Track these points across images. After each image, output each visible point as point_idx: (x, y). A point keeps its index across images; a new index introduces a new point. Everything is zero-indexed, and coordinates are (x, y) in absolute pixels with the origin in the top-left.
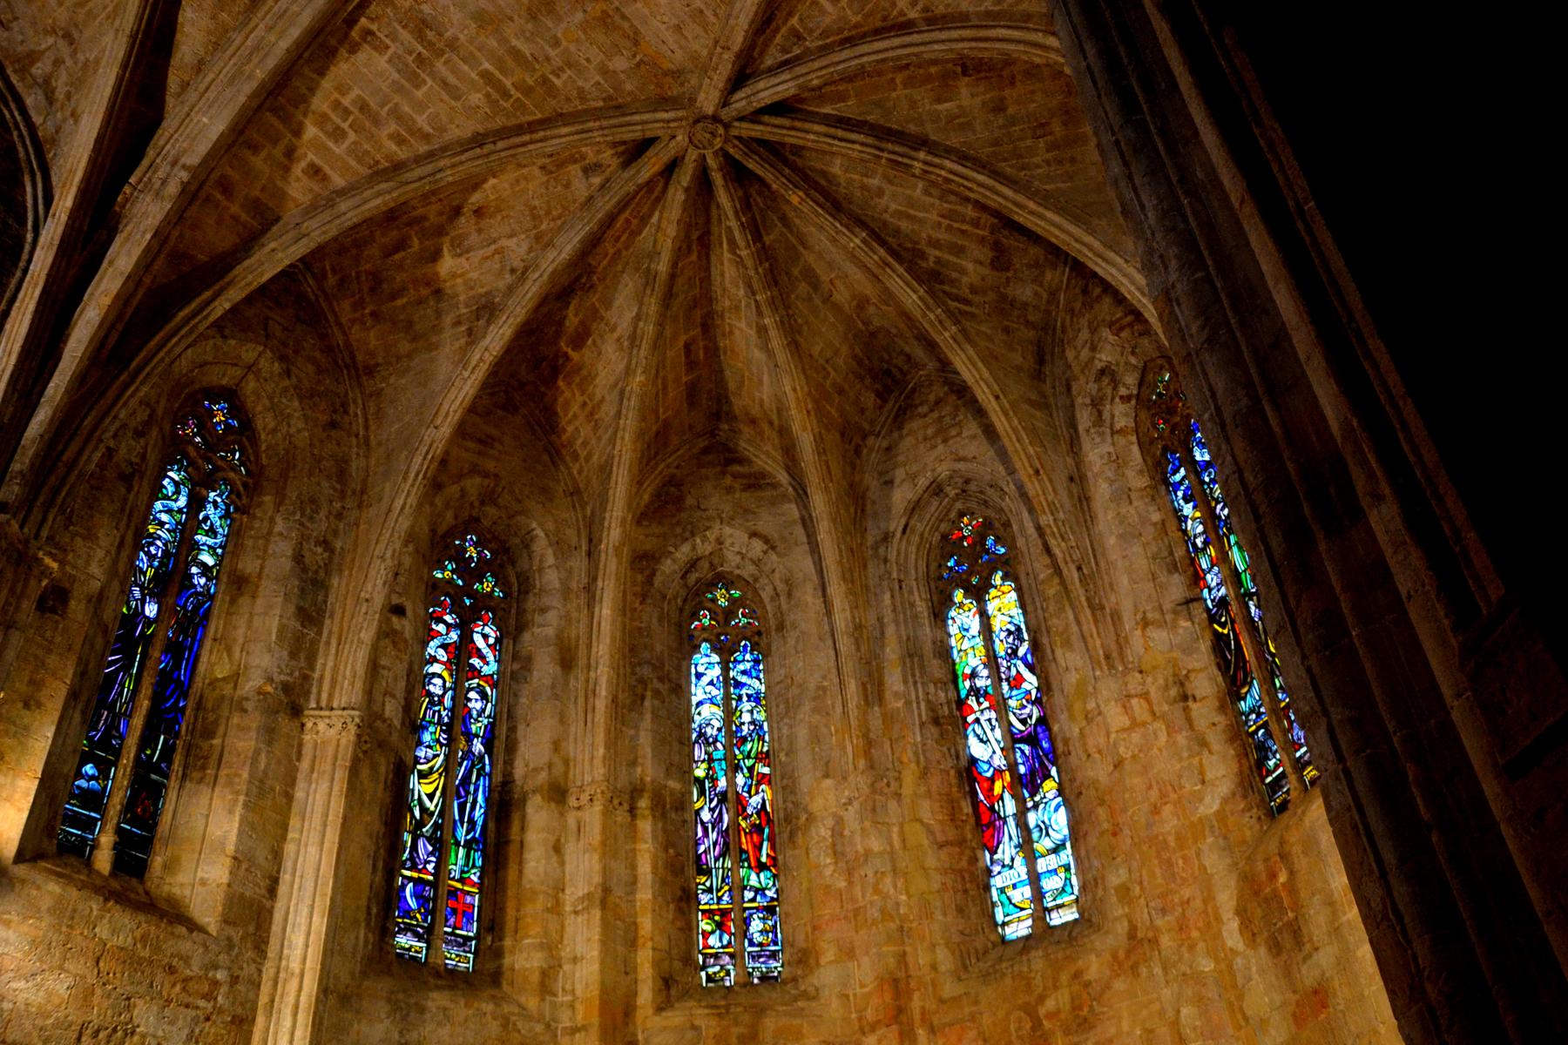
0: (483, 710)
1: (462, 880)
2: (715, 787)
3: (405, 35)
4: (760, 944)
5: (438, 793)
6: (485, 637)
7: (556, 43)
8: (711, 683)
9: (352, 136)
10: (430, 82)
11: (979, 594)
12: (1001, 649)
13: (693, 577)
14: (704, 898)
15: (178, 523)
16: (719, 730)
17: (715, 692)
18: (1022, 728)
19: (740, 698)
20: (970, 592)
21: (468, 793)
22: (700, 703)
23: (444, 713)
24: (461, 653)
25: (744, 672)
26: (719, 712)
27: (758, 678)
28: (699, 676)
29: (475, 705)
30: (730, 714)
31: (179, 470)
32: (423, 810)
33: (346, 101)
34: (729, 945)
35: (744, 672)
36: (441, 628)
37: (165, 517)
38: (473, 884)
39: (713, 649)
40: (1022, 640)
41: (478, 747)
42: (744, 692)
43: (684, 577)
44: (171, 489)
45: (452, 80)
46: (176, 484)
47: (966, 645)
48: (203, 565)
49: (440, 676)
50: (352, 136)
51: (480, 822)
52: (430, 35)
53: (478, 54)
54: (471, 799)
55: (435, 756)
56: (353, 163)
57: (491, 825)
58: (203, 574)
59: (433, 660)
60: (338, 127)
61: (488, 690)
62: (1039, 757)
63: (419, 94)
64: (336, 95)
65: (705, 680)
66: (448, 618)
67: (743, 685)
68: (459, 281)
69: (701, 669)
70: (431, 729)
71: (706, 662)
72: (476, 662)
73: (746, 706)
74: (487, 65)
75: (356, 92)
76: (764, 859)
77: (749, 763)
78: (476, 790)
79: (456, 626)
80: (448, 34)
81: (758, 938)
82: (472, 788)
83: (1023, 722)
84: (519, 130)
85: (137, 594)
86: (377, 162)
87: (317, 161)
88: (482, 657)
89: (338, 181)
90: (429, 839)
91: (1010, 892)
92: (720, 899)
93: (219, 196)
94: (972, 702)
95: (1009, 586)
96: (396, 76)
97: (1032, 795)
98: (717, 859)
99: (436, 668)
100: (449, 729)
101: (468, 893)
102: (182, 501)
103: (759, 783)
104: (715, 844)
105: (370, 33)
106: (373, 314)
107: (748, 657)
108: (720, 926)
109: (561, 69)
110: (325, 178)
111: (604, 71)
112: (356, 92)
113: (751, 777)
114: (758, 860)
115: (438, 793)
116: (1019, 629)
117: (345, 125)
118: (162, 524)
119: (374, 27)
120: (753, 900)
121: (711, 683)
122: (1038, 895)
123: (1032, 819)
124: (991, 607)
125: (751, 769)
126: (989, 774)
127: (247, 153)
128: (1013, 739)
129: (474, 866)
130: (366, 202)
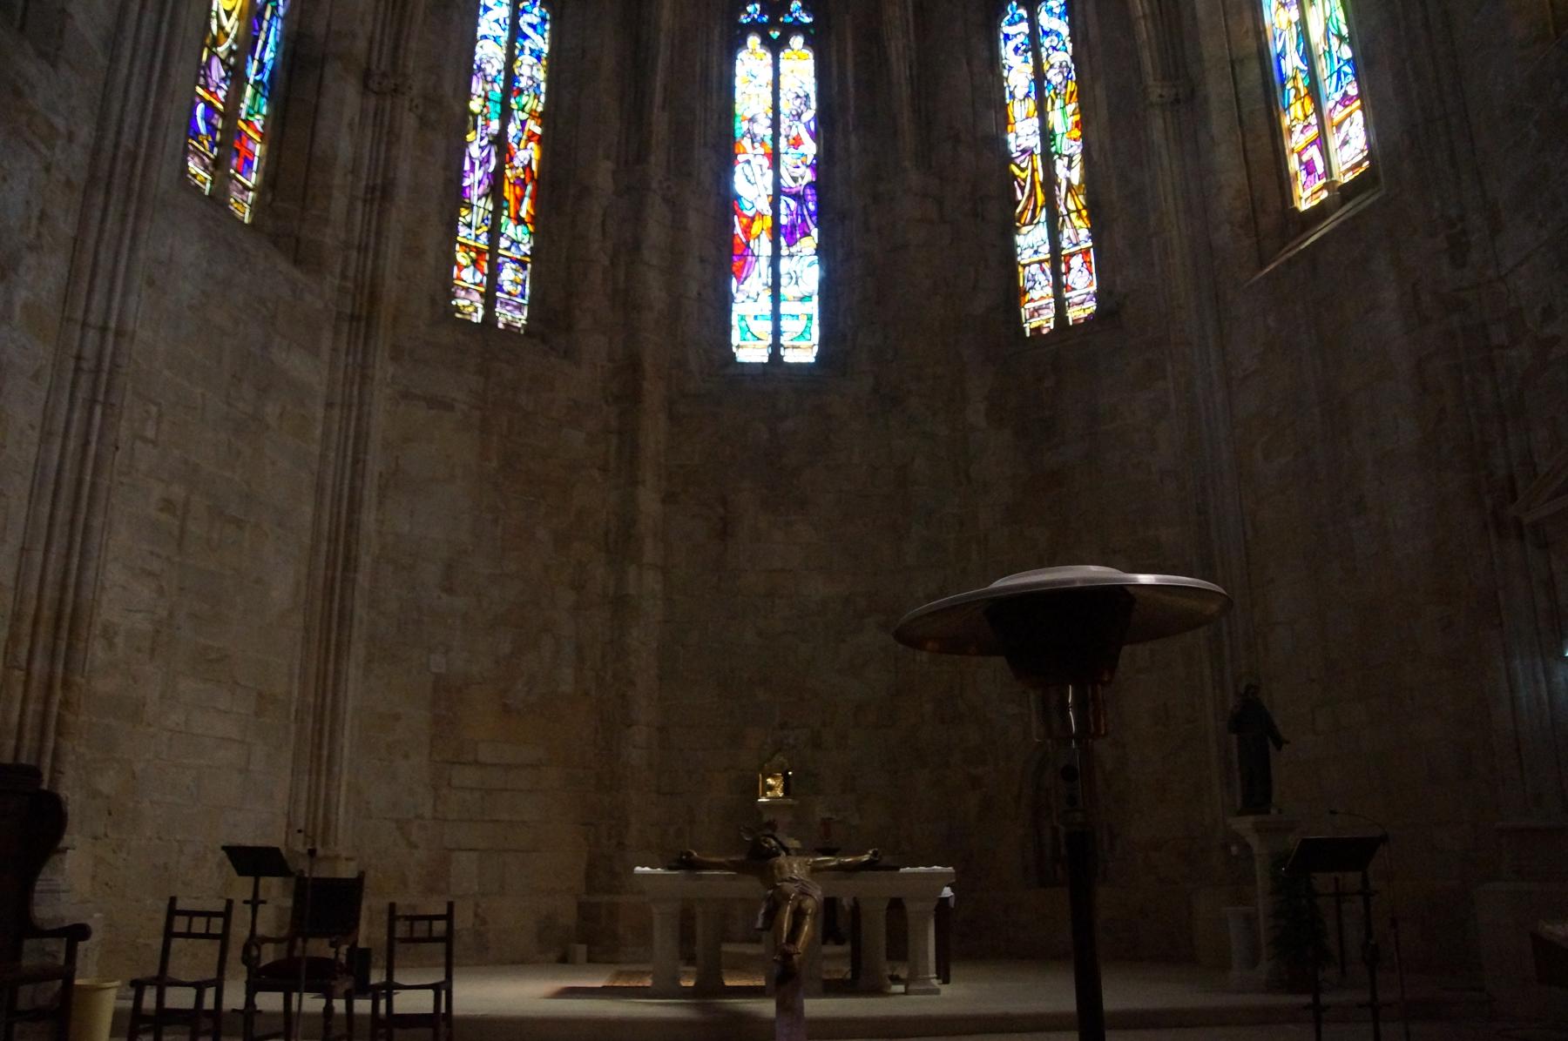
1: (246, 122)
2: (487, 126)
4: (509, 293)
5: (235, 15)
8: (497, 21)
11: (776, 48)
12: (786, 107)
14: (463, 231)
17: (499, 32)
18: (792, 184)
19: (522, 50)
20: (767, 42)
25: (531, 25)
30: (511, 59)
32: (221, 27)
34: (480, 284)
35: (531, 25)
38: (256, 131)
40: (808, 108)
42: (527, 44)
47: (751, 89)
51: (269, 67)
62: (802, 215)
65: (491, 16)
67: (526, 37)
76: (523, 214)
77: (524, 116)
78: (269, 30)
81: (507, 287)
83: (795, 179)
90: (223, 62)
91: (750, 321)
92: (477, 237)
94: (746, 142)
95: (809, 55)
97: (789, 245)
98: (479, 198)
101: (251, 138)
103: (529, 140)
104: (480, 182)
107: (536, 11)
108: (475, 262)
113: (523, 130)
114: (517, 212)
116: (807, 96)
120: (508, 249)
121: (497, 21)
122: (777, 333)
123: (785, 265)
125: (523, 123)
126: (750, 213)
128: (778, 192)
129: (258, 112)
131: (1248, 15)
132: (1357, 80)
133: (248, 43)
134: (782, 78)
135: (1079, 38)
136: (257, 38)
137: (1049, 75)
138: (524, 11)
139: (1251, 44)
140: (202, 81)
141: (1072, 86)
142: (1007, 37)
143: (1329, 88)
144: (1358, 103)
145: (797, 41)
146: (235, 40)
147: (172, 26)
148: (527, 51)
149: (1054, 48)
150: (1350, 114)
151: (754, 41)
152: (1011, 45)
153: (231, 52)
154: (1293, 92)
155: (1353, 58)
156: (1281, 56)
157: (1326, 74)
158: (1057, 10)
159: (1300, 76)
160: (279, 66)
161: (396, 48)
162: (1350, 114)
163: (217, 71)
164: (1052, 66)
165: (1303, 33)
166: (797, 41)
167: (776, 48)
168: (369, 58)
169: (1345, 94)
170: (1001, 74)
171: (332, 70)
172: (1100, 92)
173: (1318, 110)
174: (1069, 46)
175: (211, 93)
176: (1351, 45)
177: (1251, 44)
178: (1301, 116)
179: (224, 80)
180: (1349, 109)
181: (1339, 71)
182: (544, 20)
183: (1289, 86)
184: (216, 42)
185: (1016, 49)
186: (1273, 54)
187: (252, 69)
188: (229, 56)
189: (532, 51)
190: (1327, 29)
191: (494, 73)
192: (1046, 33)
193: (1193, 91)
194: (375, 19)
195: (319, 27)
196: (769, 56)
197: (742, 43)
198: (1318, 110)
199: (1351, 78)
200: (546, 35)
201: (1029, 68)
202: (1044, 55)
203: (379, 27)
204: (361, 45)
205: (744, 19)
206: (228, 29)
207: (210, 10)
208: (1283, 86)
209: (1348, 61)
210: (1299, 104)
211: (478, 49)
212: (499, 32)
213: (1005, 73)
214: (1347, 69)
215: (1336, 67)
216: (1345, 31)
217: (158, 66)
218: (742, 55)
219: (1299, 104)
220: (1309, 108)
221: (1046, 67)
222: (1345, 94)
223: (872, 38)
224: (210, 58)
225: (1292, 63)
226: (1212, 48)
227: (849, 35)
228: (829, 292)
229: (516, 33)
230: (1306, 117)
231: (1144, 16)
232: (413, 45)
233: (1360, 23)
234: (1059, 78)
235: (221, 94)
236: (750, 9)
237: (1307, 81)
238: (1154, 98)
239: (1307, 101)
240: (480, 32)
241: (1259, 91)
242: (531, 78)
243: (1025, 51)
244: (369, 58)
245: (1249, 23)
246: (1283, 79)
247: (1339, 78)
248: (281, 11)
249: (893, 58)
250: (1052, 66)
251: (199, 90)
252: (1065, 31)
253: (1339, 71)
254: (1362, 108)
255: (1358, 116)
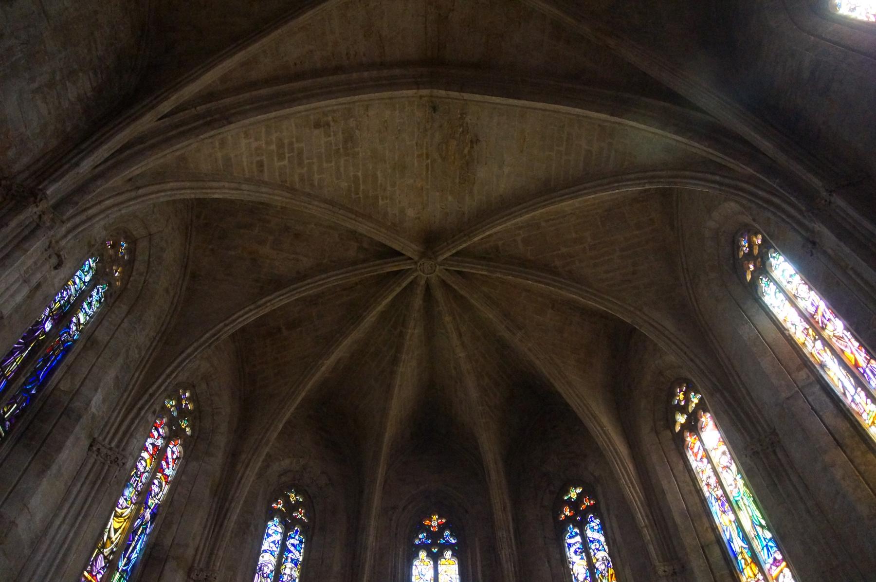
0: (157, 494)
3: (340, 136)
5: (120, 531)
6: (173, 453)
7: (393, 185)
8: (274, 542)
9: (286, 162)
10: (333, 164)
11: (435, 558)
13: (283, 479)
15: (80, 289)
16: (272, 572)
17: (274, 549)
19: (287, 559)
20: (430, 555)
21: (133, 540)
22: (265, 551)
23: (140, 484)
24: (160, 454)
25: (293, 545)
26: (274, 561)
27: (299, 551)
28: (269, 535)
29: (155, 489)
30: (279, 564)
31: (94, 261)
32: (109, 538)
33: (296, 145)
35: (293, 545)
36: (156, 434)
37: (77, 281)
39: (280, 522)
41: (148, 515)
42: (290, 555)
43: (279, 476)
44: (87, 268)
45: (342, 169)
46: (90, 267)
48: (79, 320)
49: (146, 461)
50: (286, 162)
51: (133, 562)
52: (349, 145)
53: (361, 166)
54: (134, 544)
55: (127, 507)
56: (277, 174)
57: (139, 568)
58: (76, 325)
59: (146, 450)
60: (284, 154)
61: (164, 483)
63: (325, 165)
64: (294, 140)
65: (271, 539)
66: (160, 430)
67: (290, 552)
68: (268, 261)
69: (270, 532)
70: (131, 489)
71: (275, 529)
72: (164, 463)
73: (289, 565)
74: (360, 174)
75: (302, 145)
78: (138, 541)
79: (164, 438)
80: (356, 150)
82: (137, 537)
84: (351, 211)
85: (47, 312)
86: (286, 181)
87: (265, 163)
88: (168, 463)
89: (266, 177)
90: (105, 558)
93: (217, 144)
96: (323, 150)
99: (145, 455)
100: (139, 494)
102: (87, 279)
105: (328, 125)
106: (212, 250)
109: (387, 198)
110: (262, 171)
111: (402, 211)
112: (302, 145)
115: (120, 531)
117: (287, 155)
118: (75, 283)
119: (332, 124)
121: (274, 542)
124: (440, 568)
127: (243, 135)
130: (273, 194)
131: (705, 520)
132: (779, 550)
133: (124, 547)
134: (440, 576)
135: (611, 542)
136: (130, 545)
137: (597, 565)
138: (290, 537)
139: (711, 536)
140: (89, 568)
141: (611, 571)
142: (569, 545)
143: (763, 555)
144: (784, 564)
145: (448, 554)
146: (116, 546)
147: (76, 534)
148: (289, 560)
149: (597, 549)
150: (781, 571)
151: (423, 554)
152: (572, 549)
153: (112, 552)
154: (743, 561)
155: (773, 537)
156: (730, 541)
157: (760, 548)
158: (596, 528)
159: (745, 551)
160: (139, 561)
161: (211, 554)
162: (781, 571)
163: (101, 562)
164: (597, 560)
165: (740, 527)
166: (448, 554)
167: (435, 558)
168: (194, 560)
169: (775, 559)
170: (568, 567)
171: (171, 565)
172: (628, 571)
173: (761, 570)
174: (606, 547)
175: (93, 576)
176: (769, 530)
177: (711, 536)
178: (752, 575)
179: (103, 568)
180: (779, 569)
181: (767, 545)
182: (301, 542)
183: (740, 557)
184: (104, 546)
185: (576, 552)
186: (726, 541)
187: (121, 564)
188: (110, 554)
189: (292, 560)
190: (753, 523)
191: (269, 572)
192: (592, 542)
193: (683, 567)
194: (201, 539)
195: (168, 541)
196: (432, 563)
197: (416, 556)
198: (761, 570)
199: (775, 549)
200: (302, 551)
201: (584, 563)
202: (592, 554)
203: (203, 541)
204: (190, 552)
205: (417, 542)
206: (113, 539)
207: (106, 524)
208: (736, 559)
209: (770, 539)
210: (748, 568)
211: (261, 558)
212: (274, 549)
213: (571, 566)
214: (770, 544)
215: (765, 543)
216: (763, 523)
217: (60, 556)
218: (416, 563)
219: (748, 568)
220: (756, 570)
221: (595, 561)
222: (775, 559)
223: (491, 549)
224: (98, 555)
225: (738, 544)
226: (689, 541)
227: (478, 550)
228: (813, 279)
229: (284, 549)
230: (755, 575)
231: (646, 526)
232: (221, 553)
233: (770, 516)
234: (603, 567)
235: (99, 576)
236: (421, 536)
237: (750, 554)
238: (661, 572)
239: (753, 566)
240: (263, 548)
241: (723, 562)
242: (291, 576)
243: (581, 553)
244: (194, 560)
245: (707, 525)
246: (735, 555)
247: (768, 550)
248: (148, 531)
249: (504, 561)
250: (597, 560)
251: (86, 574)
252: (602, 539)
253: (767, 545)
254: (787, 566)
255: (787, 572)
